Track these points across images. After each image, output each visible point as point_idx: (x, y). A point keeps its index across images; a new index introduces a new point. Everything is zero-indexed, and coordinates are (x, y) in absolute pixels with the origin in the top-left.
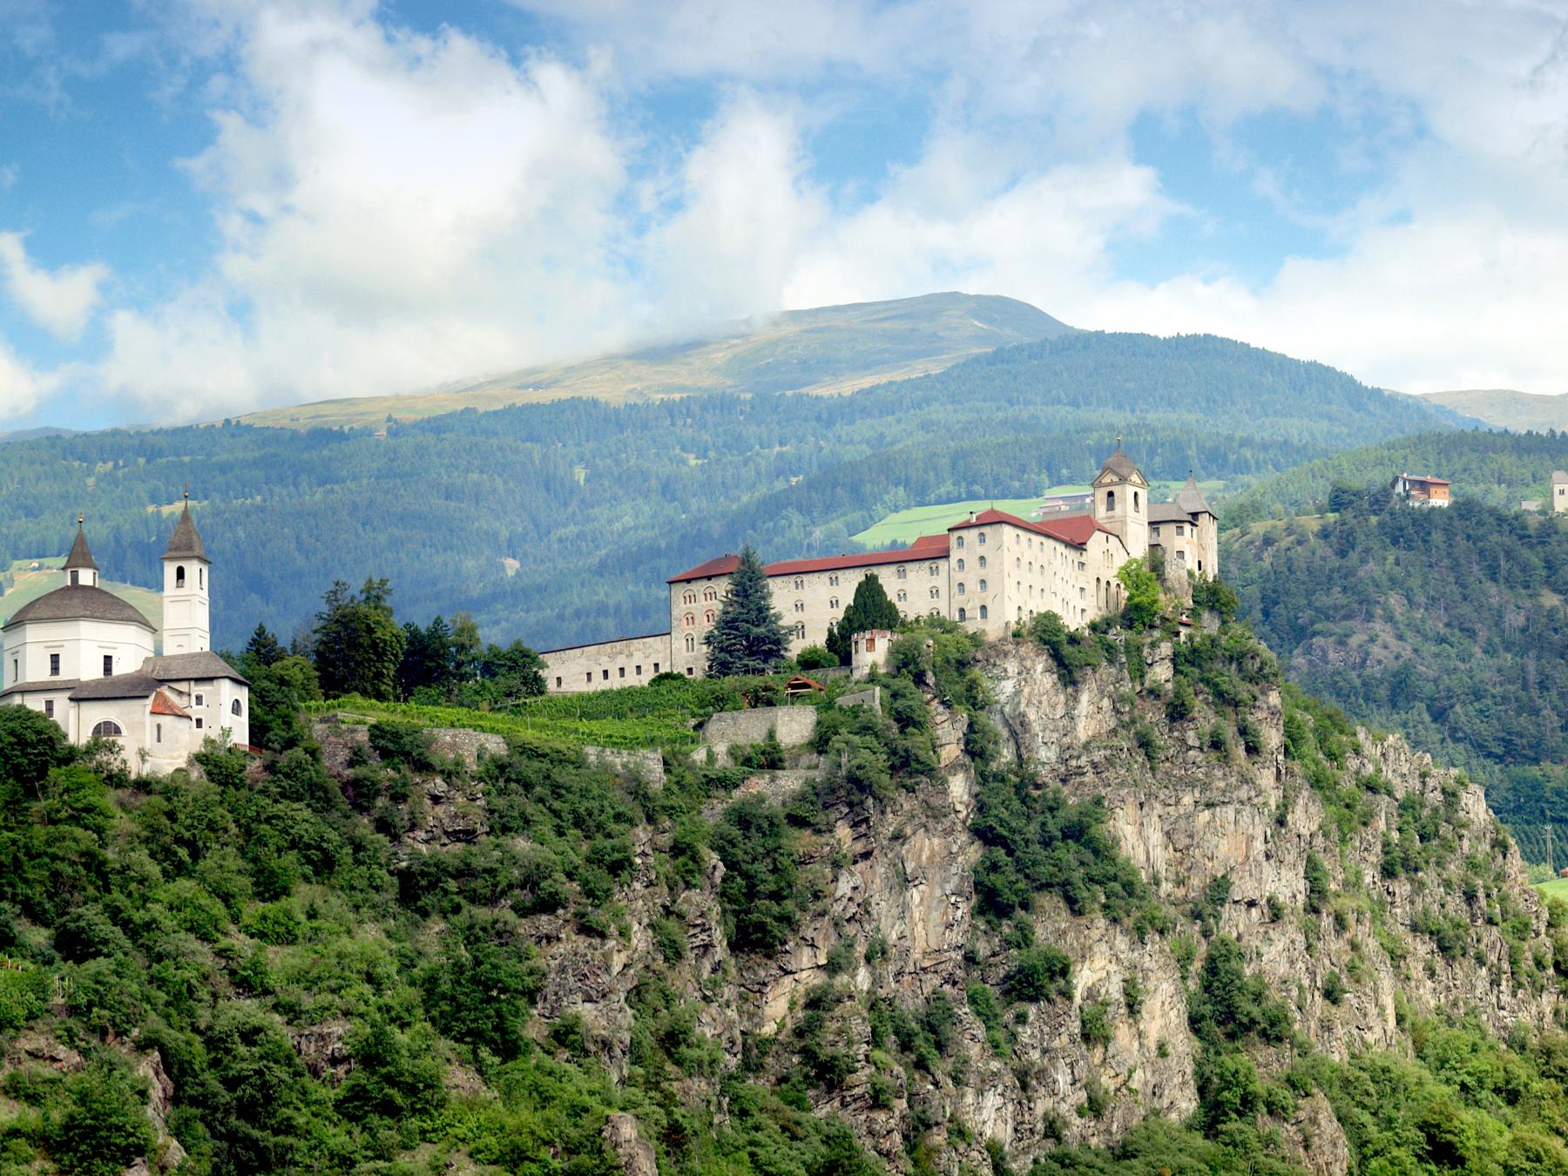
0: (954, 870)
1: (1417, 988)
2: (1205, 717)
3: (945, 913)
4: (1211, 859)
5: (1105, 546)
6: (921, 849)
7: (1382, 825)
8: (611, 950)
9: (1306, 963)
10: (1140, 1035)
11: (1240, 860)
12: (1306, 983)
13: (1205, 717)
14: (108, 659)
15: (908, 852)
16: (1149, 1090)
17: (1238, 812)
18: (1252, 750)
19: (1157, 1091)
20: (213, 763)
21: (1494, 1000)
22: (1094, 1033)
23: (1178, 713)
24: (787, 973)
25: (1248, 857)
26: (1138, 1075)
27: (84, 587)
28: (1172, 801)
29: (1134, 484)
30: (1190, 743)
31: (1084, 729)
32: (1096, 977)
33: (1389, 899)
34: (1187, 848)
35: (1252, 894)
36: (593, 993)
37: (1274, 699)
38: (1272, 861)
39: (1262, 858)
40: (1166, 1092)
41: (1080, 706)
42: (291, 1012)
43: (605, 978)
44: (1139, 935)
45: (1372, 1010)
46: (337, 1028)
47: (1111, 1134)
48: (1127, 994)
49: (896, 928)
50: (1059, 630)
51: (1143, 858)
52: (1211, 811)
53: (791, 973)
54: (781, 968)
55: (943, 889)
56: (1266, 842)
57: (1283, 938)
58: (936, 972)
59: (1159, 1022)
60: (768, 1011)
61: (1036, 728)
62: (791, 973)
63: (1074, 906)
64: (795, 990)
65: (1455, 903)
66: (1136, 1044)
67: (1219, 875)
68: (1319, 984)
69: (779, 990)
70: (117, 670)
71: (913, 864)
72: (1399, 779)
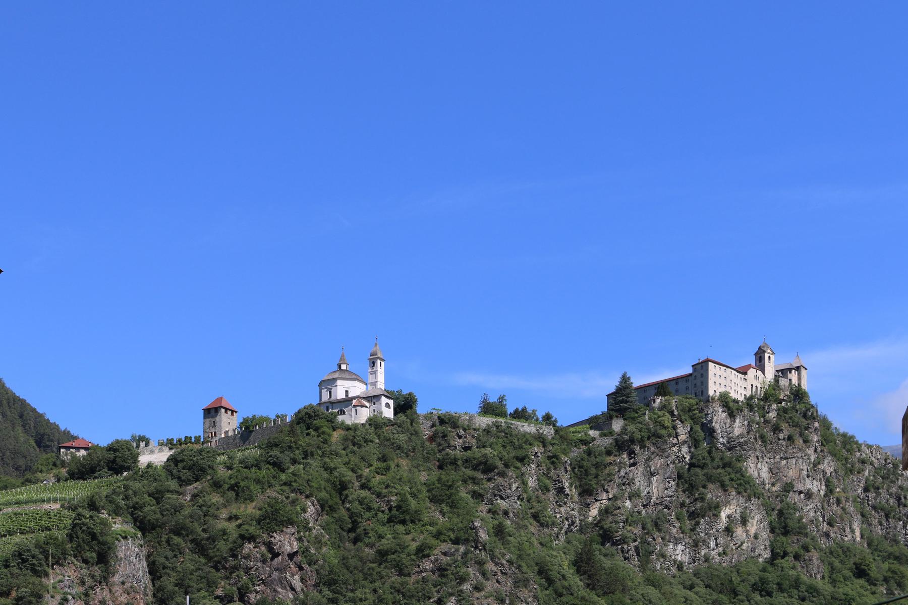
0: (668, 470)
1: (875, 528)
2: (786, 431)
3: (665, 484)
4: (786, 477)
5: (756, 374)
6: (657, 463)
7: (867, 473)
8: (512, 482)
9: (821, 513)
10: (747, 531)
11: (797, 477)
12: (821, 519)
13: (786, 431)
14: (347, 392)
15: (652, 464)
16: (750, 549)
17: (796, 460)
18: (806, 441)
19: (753, 550)
20: (375, 423)
21: (904, 532)
22: (728, 530)
23: (776, 429)
24: (597, 500)
25: (800, 476)
26: (745, 545)
27: (342, 370)
28: (772, 457)
29: (769, 353)
30: (780, 438)
31: (737, 431)
32: (731, 511)
33: (867, 498)
34: (777, 473)
35: (802, 489)
36: (504, 496)
37: (816, 425)
38: (810, 478)
39: (805, 476)
40: (757, 551)
41: (735, 424)
42: (379, 495)
43: (509, 491)
44: (749, 499)
45: (848, 530)
46: (394, 498)
47: (732, 562)
48: (742, 517)
49: (647, 489)
50: (729, 397)
51: (757, 475)
52: (787, 460)
53: (599, 500)
54: (595, 499)
55: (664, 476)
56: (808, 471)
57: (812, 504)
58: (661, 505)
59: (755, 527)
60: (590, 514)
61: (719, 431)
62: (599, 500)
63: (723, 487)
64: (601, 506)
65: (892, 502)
66: (745, 534)
67: (789, 482)
68: (826, 519)
69: (595, 506)
70: (350, 395)
71: (654, 468)
72: (877, 460)
